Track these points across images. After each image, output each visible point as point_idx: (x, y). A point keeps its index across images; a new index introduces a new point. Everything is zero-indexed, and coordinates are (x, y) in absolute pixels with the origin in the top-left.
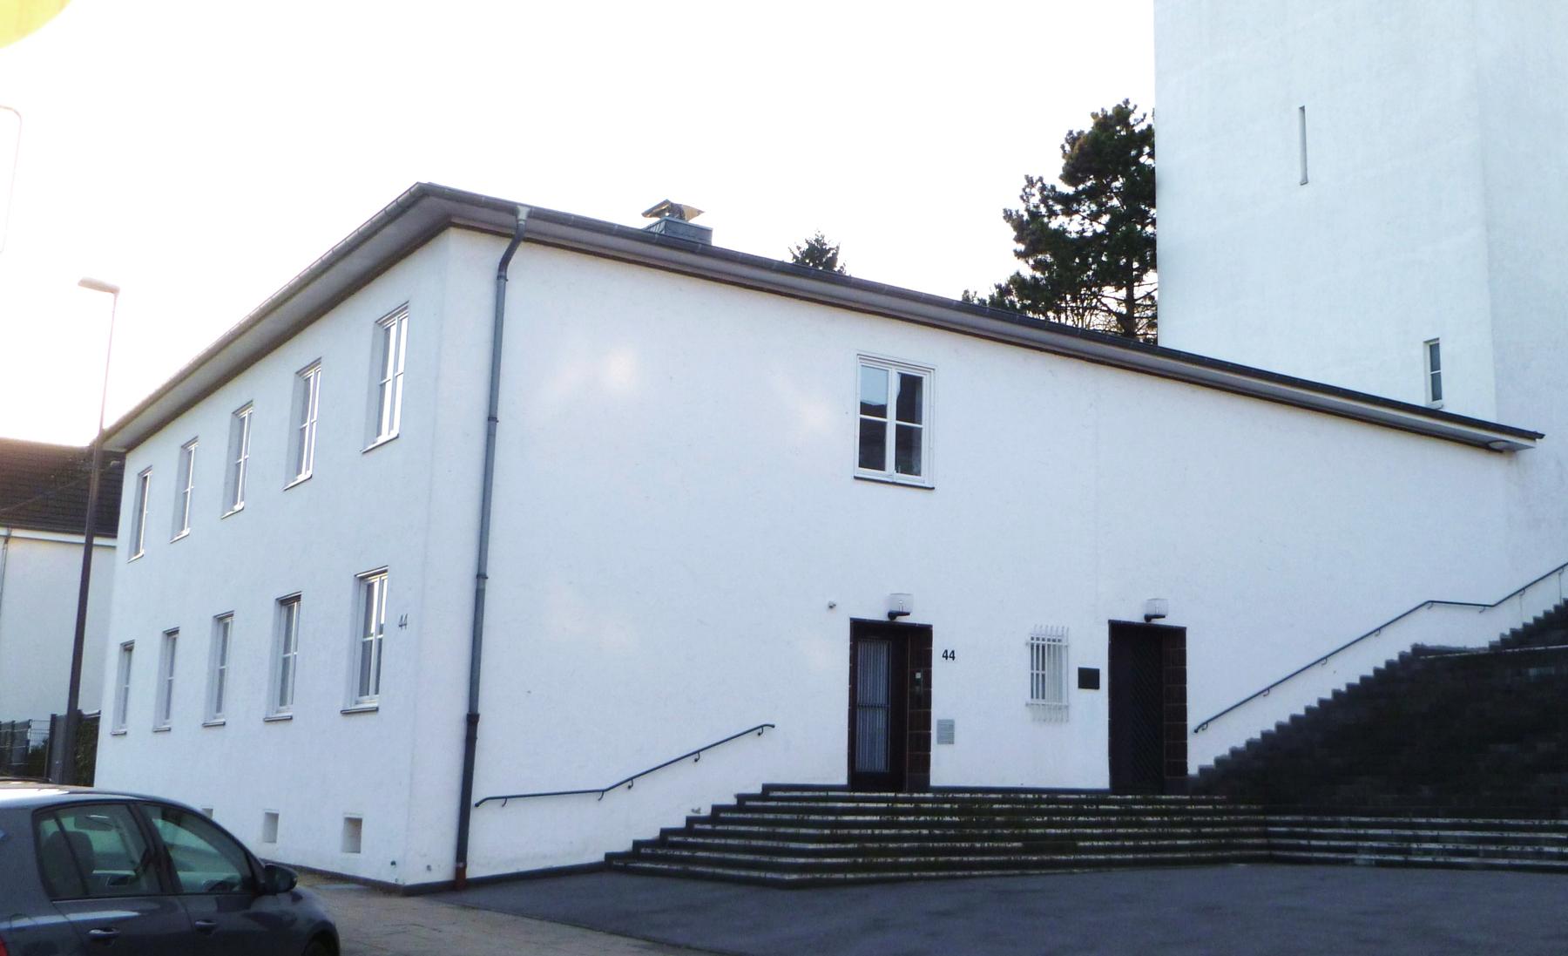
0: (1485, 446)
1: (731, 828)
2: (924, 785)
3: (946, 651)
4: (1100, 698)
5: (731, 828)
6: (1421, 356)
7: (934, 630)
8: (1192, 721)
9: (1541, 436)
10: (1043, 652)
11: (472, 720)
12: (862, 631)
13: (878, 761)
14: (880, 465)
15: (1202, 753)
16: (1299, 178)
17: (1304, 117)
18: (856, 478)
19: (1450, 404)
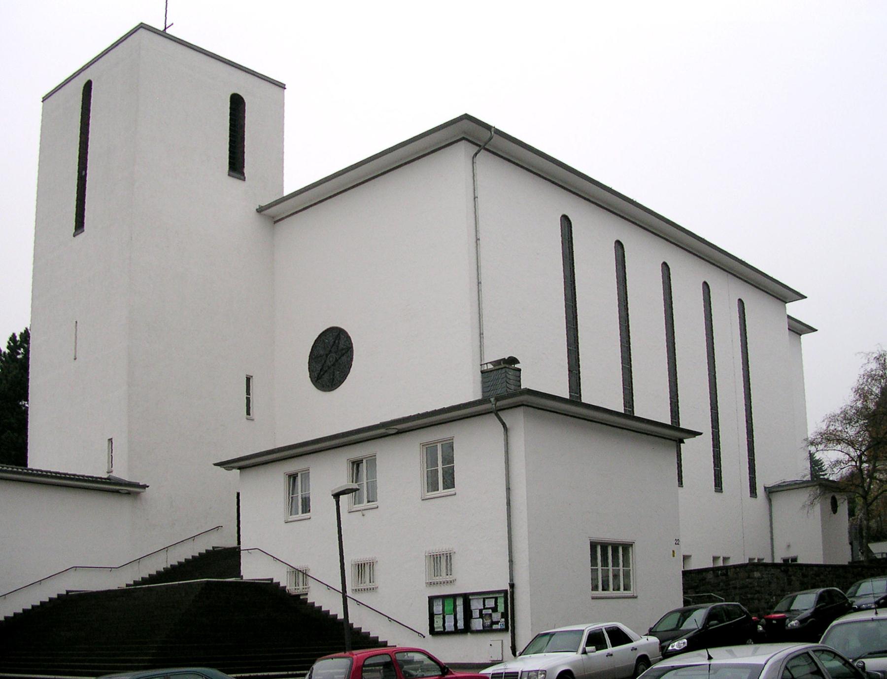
6: (106, 443)
9: (148, 487)
16: (74, 358)
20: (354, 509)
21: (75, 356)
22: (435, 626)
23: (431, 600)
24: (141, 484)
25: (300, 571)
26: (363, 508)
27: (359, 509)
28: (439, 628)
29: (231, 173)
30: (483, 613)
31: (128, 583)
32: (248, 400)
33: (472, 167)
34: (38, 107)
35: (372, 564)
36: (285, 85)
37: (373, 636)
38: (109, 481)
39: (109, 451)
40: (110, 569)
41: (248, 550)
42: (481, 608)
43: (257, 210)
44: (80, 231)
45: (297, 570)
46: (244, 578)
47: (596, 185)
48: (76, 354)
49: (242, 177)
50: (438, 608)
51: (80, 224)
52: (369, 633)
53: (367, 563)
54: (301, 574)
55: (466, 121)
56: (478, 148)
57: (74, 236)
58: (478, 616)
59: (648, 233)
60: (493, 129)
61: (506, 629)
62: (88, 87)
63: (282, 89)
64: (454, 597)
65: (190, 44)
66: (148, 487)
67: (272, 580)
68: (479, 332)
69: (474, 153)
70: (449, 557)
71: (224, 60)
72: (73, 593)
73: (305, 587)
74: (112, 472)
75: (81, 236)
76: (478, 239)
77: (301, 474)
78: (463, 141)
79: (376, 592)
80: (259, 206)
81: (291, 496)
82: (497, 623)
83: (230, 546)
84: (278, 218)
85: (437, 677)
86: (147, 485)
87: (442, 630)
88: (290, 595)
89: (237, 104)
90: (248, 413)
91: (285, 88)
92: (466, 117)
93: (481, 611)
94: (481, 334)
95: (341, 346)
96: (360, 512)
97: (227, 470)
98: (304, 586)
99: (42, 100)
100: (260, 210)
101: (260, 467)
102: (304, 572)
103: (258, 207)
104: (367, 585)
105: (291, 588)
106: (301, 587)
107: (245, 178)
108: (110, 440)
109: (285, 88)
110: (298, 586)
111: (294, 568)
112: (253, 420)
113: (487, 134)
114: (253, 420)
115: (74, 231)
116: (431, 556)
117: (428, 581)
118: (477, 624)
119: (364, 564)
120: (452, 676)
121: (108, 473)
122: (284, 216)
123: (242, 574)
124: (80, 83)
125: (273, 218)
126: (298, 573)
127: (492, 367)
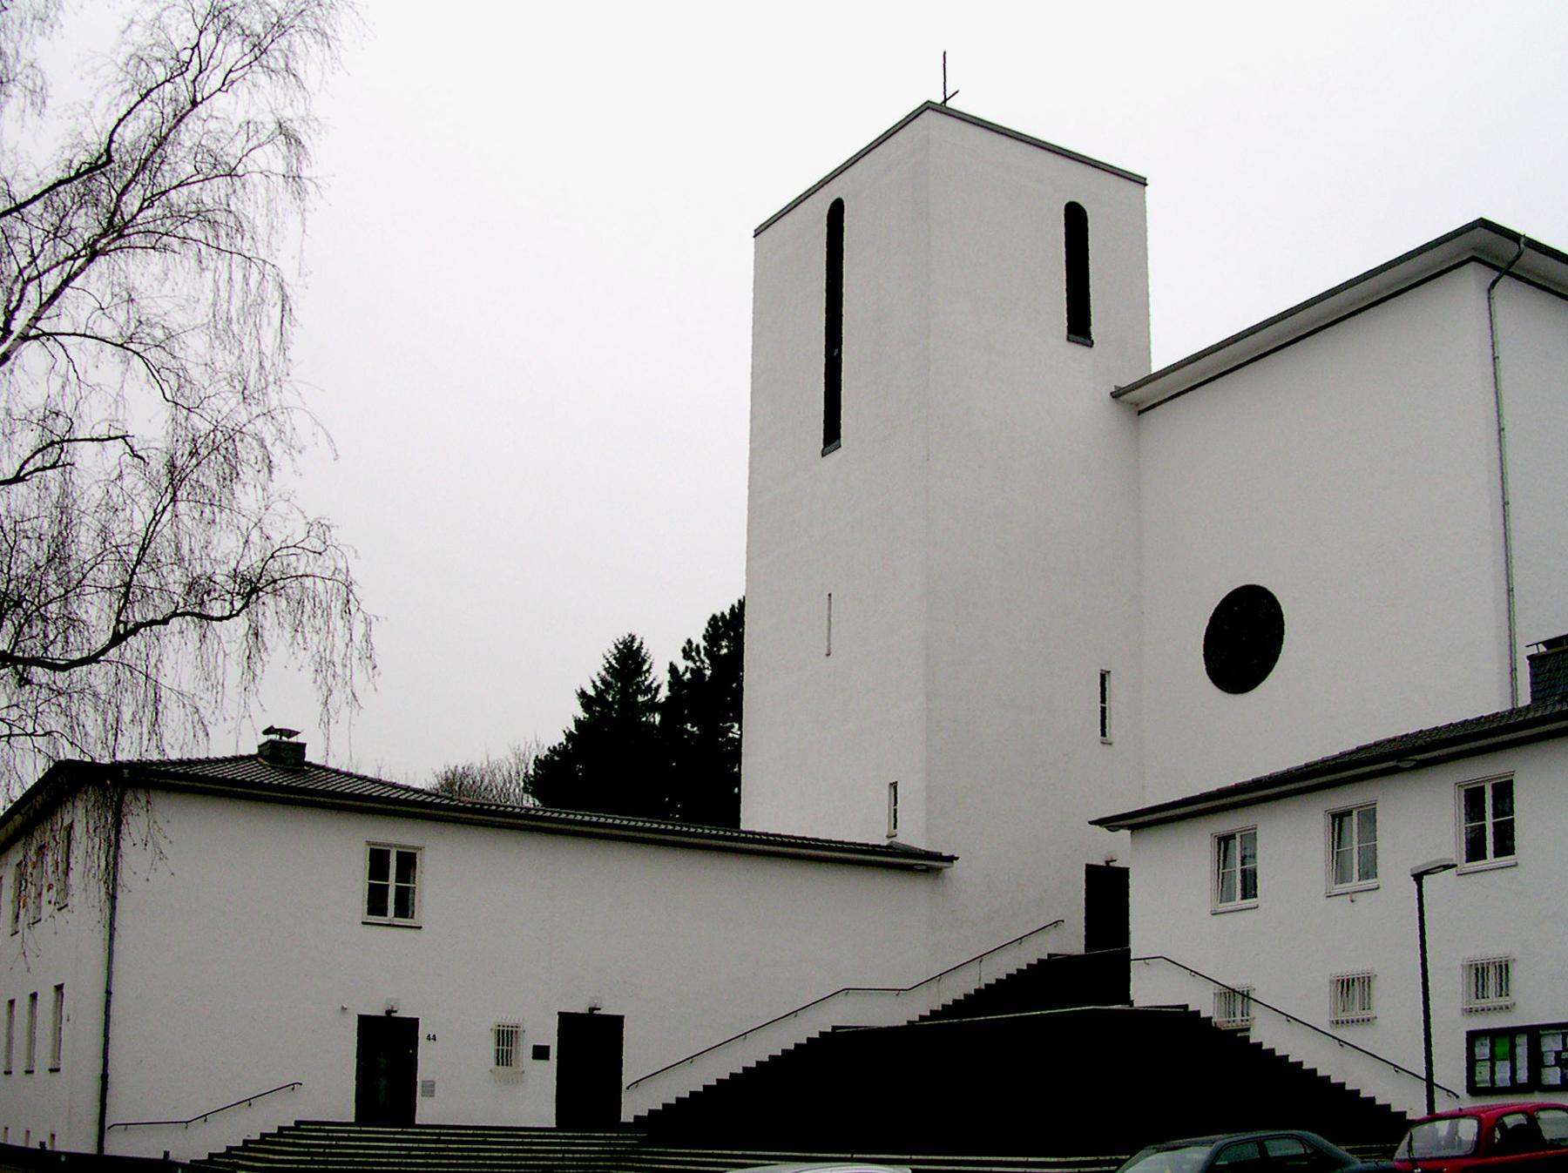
3: (429, 1036)
4: (550, 1067)
6: (886, 792)
8: (626, 1080)
9: (957, 858)
10: (506, 1038)
11: (105, 1077)
12: (367, 1025)
14: (384, 914)
15: (633, 1106)
16: (826, 651)
17: (830, 603)
18: (363, 923)
20: (1336, 892)
21: (829, 650)
22: (1477, 1079)
23: (1473, 1037)
24: (944, 854)
25: (1238, 992)
26: (1353, 889)
27: (1344, 891)
28: (1483, 1082)
29: (1071, 336)
30: (1563, 1057)
31: (923, 1014)
32: (1103, 710)
33: (1487, 304)
34: (747, 246)
35: (1366, 980)
36: (1145, 179)
37: (1365, 1096)
38: (891, 850)
39: (890, 803)
40: (897, 992)
41: (1145, 959)
42: (1558, 1049)
43: (1111, 394)
44: (833, 446)
45: (1233, 990)
46: (1136, 1005)
47: (1390, 268)
48: (829, 644)
49: (1089, 342)
50: (1483, 1050)
51: (832, 434)
53: (1358, 978)
54: (1236, 996)
55: (1482, 231)
56: (1497, 274)
57: (823, 455)
58: (1553, 1063)
59: (1326, 330)
60: (1523, 240)
62: (836, 212)
63: (1140, 186)
64: (1511, 1033)
65: (1004, 128)
66: (957, 858)
67: (1186, 1007)
68: (1506, 587)
69: (1491, 281)
70: (1503, 969)
71: (1037, 143)
72: (851, 1030)
73: (1246, 1018)
74: (895, 836)
75: (835, 456)
76: (1501, 430)
77: (1241, 836)
78: (1473, 263)
79: (1373, 1024)
80: (1116, 387)
81: (1221, 871)
83: (1078, 953)
84: (1148, 405)
86: (956, 856)
87: (1489, 1085)
88: (1216, 1030)
89: (1076, 218)
90: (1103, 734)
91: (1146, 185)
92: (1483, 223)
93: (1558, 1054)
94: (1510, 591)
96: (1349, 895)
97: (1109, 830)
98: (1243, 1016)
99: (753, 234)
100: (1117, 394)
102: (1245, 993)
103: (1113, 390)
104: (1356, 1013)
105: (1219, 1019)
106: (1239, 1017)
107: (1093, 342)
108: (894, 785)
109: (1146, 185)
110: (1234, 1016)
111: (1227, 987)
112: (1110, 744)
113: (1511, 249)
114: (1110, 744)
115: (822, 447)
116: (1471, 965)
117: (1465, 1007)
119: (1353, 980)
120: (1348, 1147)
121: (888, 837)
122: (1156, 401)
123: (1132, 998)
124: (822, 203)
125: (1137, 405)
126: (1234, 995)
127: (1545, 649)
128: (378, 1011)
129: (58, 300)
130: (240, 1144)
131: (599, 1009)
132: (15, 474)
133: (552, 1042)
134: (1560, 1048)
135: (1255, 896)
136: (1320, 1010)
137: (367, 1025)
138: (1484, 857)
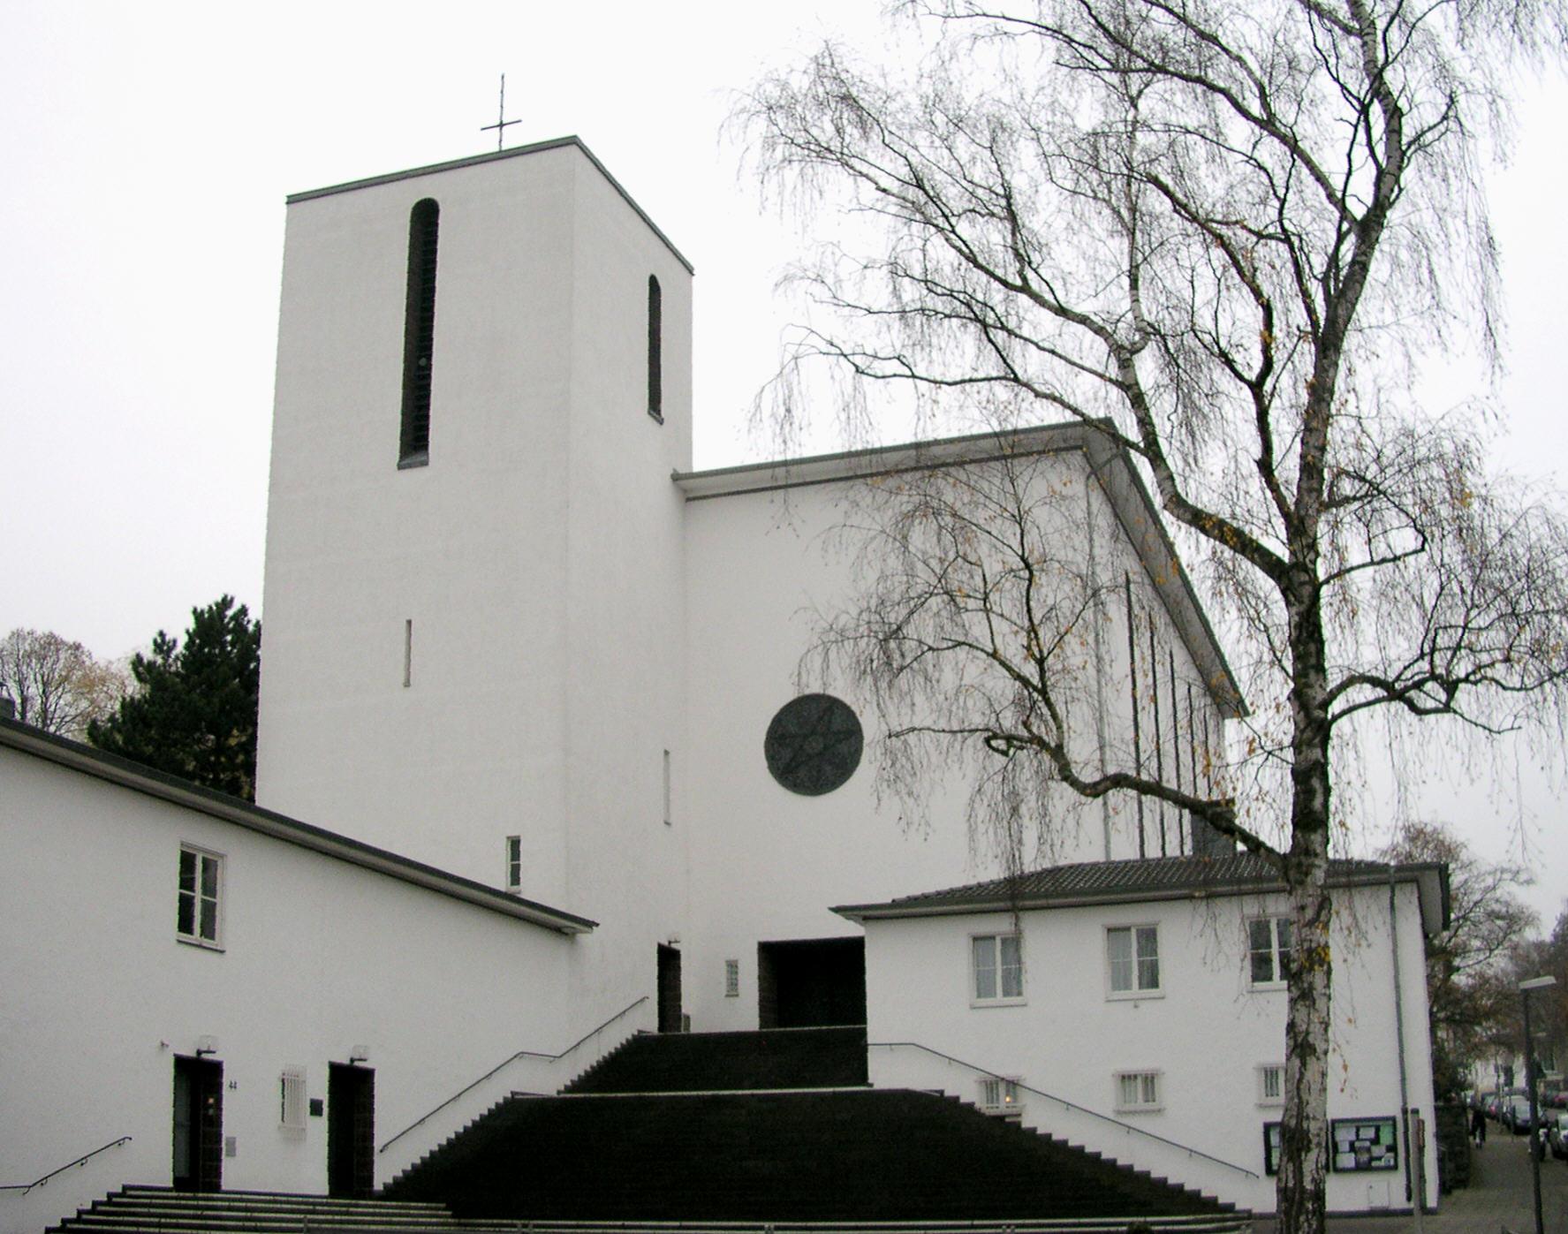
0: (558, 930)
1: (141, 1219)
2: (216, 1187)
5: (141, 1219)
7: (225, 1067)
9: (597, 925)
10: (287, 1084)
12: (181, 1064)
13: (184, 1173)
16: (402, 679)
19: (528, 891)
51: (415, 439)
52: (1149, 1173)
61: (1395, 1167)
66: (597, 925)
67: (942, 1092)
82: (1379, 1158)
85: (1124, 1228)
93: (1352, 1144)
95: (836, 727)
101: (312, 855)
105: (981, 1104)
118: (1347, 1160)
128: (189, 1052)
129: (1280, 637)
130: (120, 1190)
131: (365, 1060)
132: (1330, 747)
133: (323, 1095)
134: (1353, 1137)
135: (1020, 994)
136: (1105, 1099)
137: (181, 1064)
138: (1270, 978)
